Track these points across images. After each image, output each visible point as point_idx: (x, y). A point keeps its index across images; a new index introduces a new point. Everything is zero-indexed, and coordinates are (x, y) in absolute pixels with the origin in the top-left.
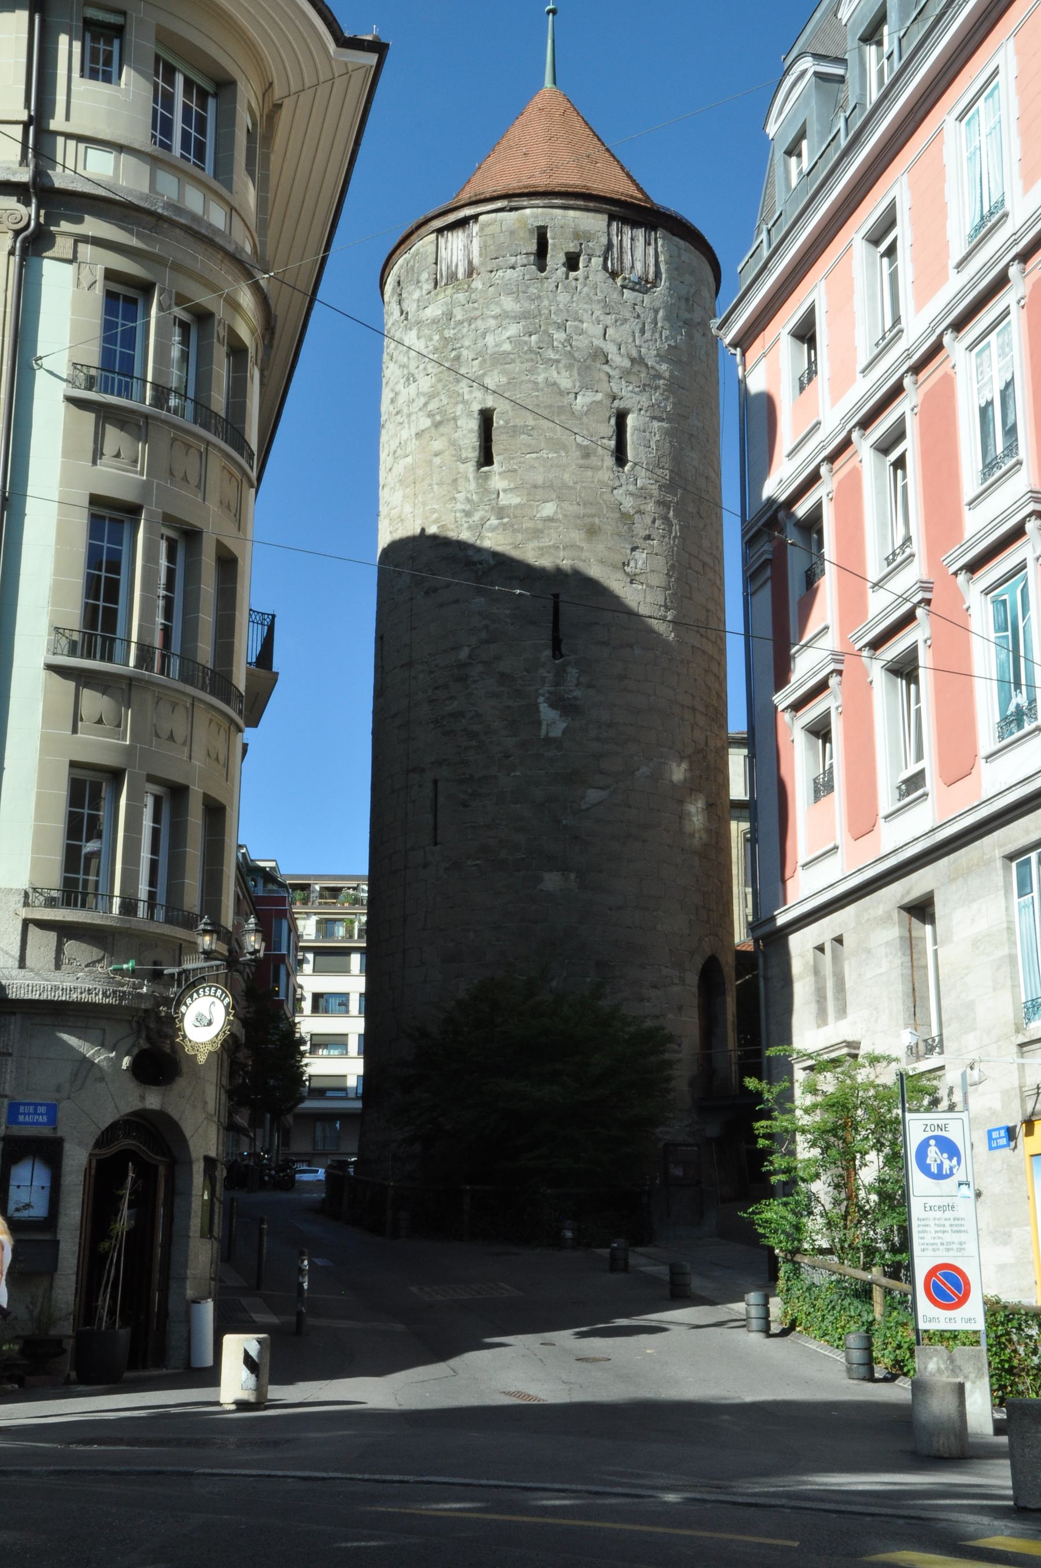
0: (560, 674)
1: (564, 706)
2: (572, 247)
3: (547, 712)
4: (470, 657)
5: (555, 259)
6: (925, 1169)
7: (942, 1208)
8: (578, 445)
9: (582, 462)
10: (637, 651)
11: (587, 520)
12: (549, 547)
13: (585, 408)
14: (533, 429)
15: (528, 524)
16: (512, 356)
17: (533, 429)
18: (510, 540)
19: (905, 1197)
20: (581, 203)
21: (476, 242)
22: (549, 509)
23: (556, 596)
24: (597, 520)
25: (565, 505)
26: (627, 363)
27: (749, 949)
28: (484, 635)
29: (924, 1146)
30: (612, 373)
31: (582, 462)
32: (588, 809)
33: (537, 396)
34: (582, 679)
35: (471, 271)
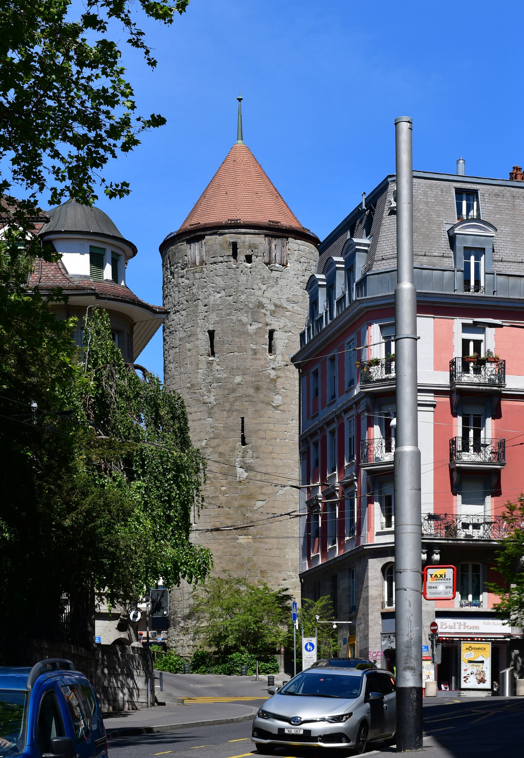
0: (245, 452)
1: (248, 468)
2: (249, 252)
3: (240, 470)
4: (206, 444)
5: (241, 257)
6: (307, 649)
7: (310, 658)
8: (252, 349)
9: (253, 357)
10: (278, 440)
11: (256, 383)
12: (239, 396)
13: (255, 331)
14: (231, 342)
15: (230, 386)
16: (221, 306)
17: (231, 342)
18: (222, 393)
19: (301, 655)
20: (252, 231)
21: (204, 249)
22: (238, 379)
23: (243, 419)
24: (260, 383)
25: (246, 377)
26: (273, 308)
27: (76, 713)
28: (212, 435)
29: (307, 644)
30: (266, 313)
31: (253, 357)
32: (257, 510)
33: (233, 326)
34: (254, 455)
35: (202, 262)
